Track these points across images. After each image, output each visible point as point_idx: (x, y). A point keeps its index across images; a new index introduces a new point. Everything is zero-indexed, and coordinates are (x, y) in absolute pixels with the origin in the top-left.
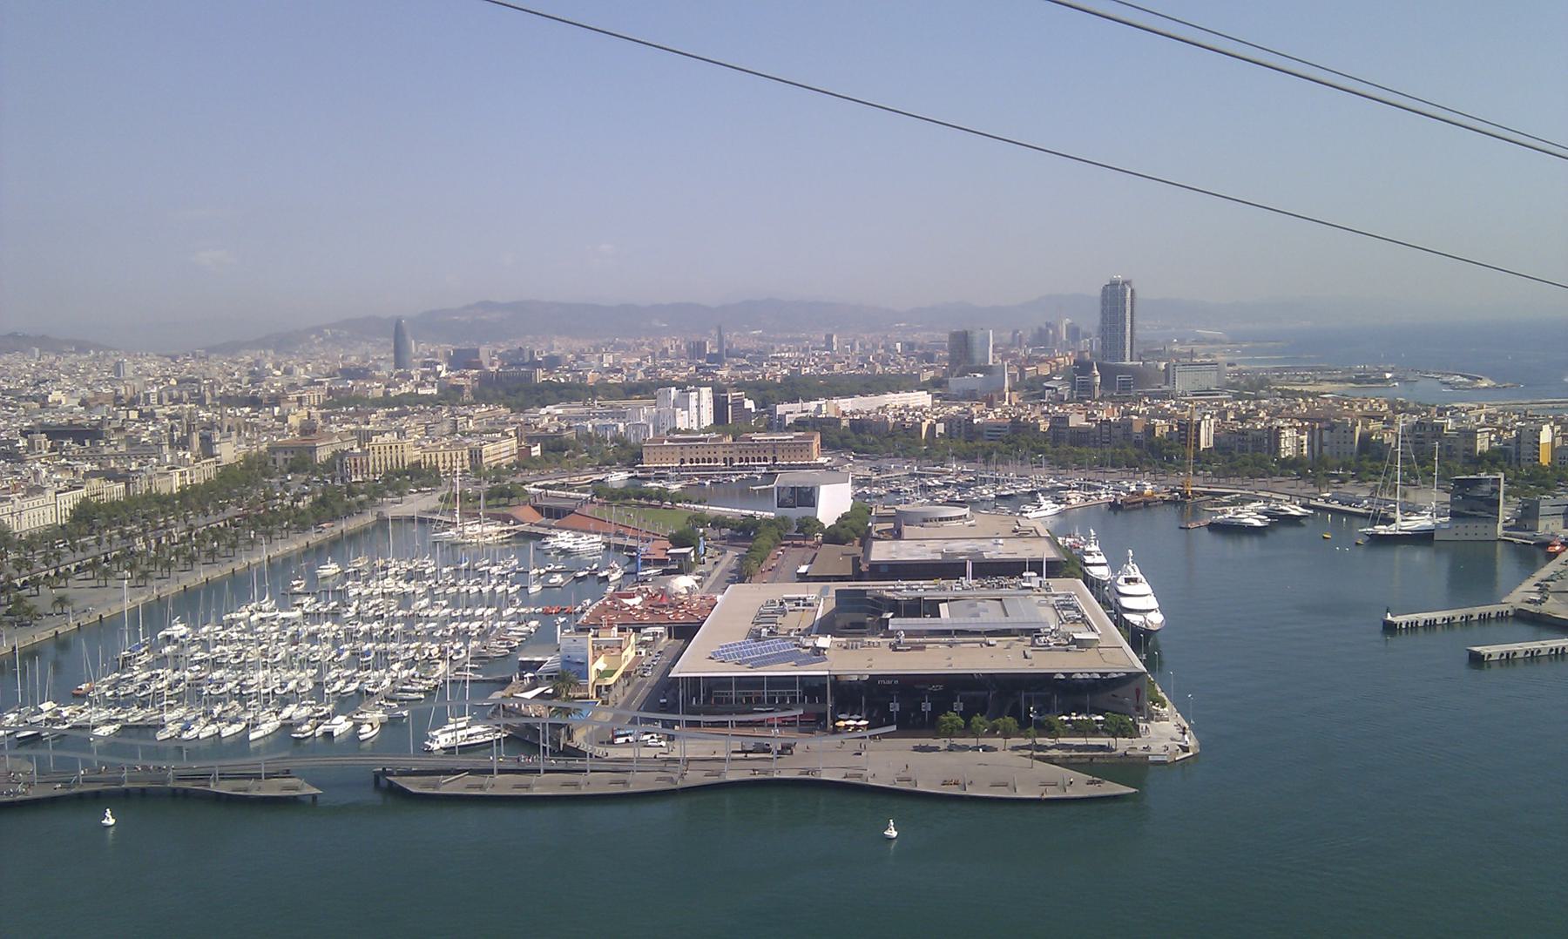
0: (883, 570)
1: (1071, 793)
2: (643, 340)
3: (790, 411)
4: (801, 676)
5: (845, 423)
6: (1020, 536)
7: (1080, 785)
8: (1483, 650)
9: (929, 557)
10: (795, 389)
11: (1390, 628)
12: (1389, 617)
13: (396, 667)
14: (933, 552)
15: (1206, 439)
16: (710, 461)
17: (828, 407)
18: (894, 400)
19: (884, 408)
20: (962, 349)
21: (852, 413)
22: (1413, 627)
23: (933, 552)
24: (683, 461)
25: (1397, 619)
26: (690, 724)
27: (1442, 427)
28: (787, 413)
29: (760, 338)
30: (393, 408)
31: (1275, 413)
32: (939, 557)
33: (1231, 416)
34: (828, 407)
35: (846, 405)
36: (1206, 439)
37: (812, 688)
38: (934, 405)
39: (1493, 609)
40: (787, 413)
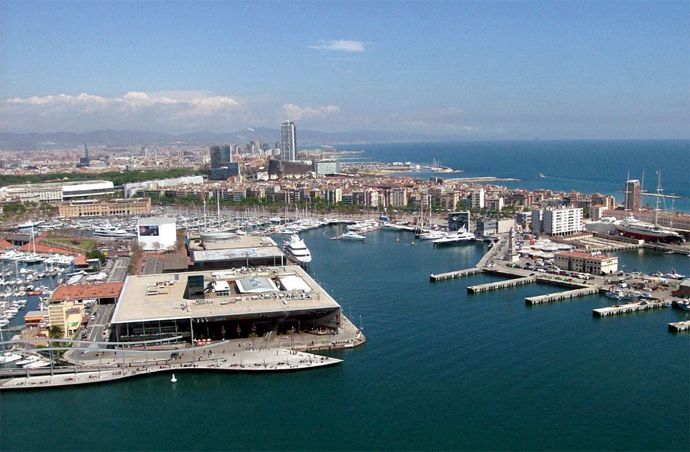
0: (202, 265)
1: (314, 365)
2: (43, 151)
3: (132, 188)
4: (177, 320)
5: (162, 193)
6: (264, 246)
7: (317, 361)
8: (474, 288)
9: (223, 258)
10: (133, 176)
11: (433, 280)
12: (432, 276)
13: (606, 422)
14: (225, 255)
15: (338, 198)
16: (92, 214)
17: (151, 185)
18: (186, 180)
19: (182, 185)
20: (219, 155)
21: (165, 188)
22: (442, 280)
23: (225, 255)
24: (80, 214)
25: (436, 276)
26: (121, 346)
27: (439, 191)
28: (133, 188)
29: (105, 150)
30: (76, 94)
31: (367, 186)
32: (228, 258)
33: (347, 186)
34: (151, 185)
35: (162, 183)
36: (338, 198)
37: (183, 325)
38: (205, 183)
39: (473, 270)
40: (133, 188)
